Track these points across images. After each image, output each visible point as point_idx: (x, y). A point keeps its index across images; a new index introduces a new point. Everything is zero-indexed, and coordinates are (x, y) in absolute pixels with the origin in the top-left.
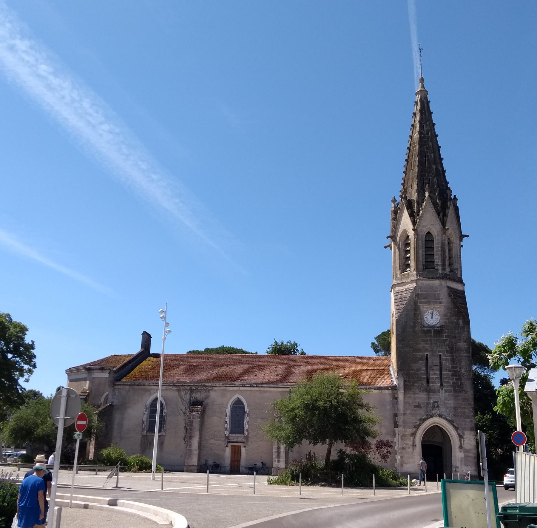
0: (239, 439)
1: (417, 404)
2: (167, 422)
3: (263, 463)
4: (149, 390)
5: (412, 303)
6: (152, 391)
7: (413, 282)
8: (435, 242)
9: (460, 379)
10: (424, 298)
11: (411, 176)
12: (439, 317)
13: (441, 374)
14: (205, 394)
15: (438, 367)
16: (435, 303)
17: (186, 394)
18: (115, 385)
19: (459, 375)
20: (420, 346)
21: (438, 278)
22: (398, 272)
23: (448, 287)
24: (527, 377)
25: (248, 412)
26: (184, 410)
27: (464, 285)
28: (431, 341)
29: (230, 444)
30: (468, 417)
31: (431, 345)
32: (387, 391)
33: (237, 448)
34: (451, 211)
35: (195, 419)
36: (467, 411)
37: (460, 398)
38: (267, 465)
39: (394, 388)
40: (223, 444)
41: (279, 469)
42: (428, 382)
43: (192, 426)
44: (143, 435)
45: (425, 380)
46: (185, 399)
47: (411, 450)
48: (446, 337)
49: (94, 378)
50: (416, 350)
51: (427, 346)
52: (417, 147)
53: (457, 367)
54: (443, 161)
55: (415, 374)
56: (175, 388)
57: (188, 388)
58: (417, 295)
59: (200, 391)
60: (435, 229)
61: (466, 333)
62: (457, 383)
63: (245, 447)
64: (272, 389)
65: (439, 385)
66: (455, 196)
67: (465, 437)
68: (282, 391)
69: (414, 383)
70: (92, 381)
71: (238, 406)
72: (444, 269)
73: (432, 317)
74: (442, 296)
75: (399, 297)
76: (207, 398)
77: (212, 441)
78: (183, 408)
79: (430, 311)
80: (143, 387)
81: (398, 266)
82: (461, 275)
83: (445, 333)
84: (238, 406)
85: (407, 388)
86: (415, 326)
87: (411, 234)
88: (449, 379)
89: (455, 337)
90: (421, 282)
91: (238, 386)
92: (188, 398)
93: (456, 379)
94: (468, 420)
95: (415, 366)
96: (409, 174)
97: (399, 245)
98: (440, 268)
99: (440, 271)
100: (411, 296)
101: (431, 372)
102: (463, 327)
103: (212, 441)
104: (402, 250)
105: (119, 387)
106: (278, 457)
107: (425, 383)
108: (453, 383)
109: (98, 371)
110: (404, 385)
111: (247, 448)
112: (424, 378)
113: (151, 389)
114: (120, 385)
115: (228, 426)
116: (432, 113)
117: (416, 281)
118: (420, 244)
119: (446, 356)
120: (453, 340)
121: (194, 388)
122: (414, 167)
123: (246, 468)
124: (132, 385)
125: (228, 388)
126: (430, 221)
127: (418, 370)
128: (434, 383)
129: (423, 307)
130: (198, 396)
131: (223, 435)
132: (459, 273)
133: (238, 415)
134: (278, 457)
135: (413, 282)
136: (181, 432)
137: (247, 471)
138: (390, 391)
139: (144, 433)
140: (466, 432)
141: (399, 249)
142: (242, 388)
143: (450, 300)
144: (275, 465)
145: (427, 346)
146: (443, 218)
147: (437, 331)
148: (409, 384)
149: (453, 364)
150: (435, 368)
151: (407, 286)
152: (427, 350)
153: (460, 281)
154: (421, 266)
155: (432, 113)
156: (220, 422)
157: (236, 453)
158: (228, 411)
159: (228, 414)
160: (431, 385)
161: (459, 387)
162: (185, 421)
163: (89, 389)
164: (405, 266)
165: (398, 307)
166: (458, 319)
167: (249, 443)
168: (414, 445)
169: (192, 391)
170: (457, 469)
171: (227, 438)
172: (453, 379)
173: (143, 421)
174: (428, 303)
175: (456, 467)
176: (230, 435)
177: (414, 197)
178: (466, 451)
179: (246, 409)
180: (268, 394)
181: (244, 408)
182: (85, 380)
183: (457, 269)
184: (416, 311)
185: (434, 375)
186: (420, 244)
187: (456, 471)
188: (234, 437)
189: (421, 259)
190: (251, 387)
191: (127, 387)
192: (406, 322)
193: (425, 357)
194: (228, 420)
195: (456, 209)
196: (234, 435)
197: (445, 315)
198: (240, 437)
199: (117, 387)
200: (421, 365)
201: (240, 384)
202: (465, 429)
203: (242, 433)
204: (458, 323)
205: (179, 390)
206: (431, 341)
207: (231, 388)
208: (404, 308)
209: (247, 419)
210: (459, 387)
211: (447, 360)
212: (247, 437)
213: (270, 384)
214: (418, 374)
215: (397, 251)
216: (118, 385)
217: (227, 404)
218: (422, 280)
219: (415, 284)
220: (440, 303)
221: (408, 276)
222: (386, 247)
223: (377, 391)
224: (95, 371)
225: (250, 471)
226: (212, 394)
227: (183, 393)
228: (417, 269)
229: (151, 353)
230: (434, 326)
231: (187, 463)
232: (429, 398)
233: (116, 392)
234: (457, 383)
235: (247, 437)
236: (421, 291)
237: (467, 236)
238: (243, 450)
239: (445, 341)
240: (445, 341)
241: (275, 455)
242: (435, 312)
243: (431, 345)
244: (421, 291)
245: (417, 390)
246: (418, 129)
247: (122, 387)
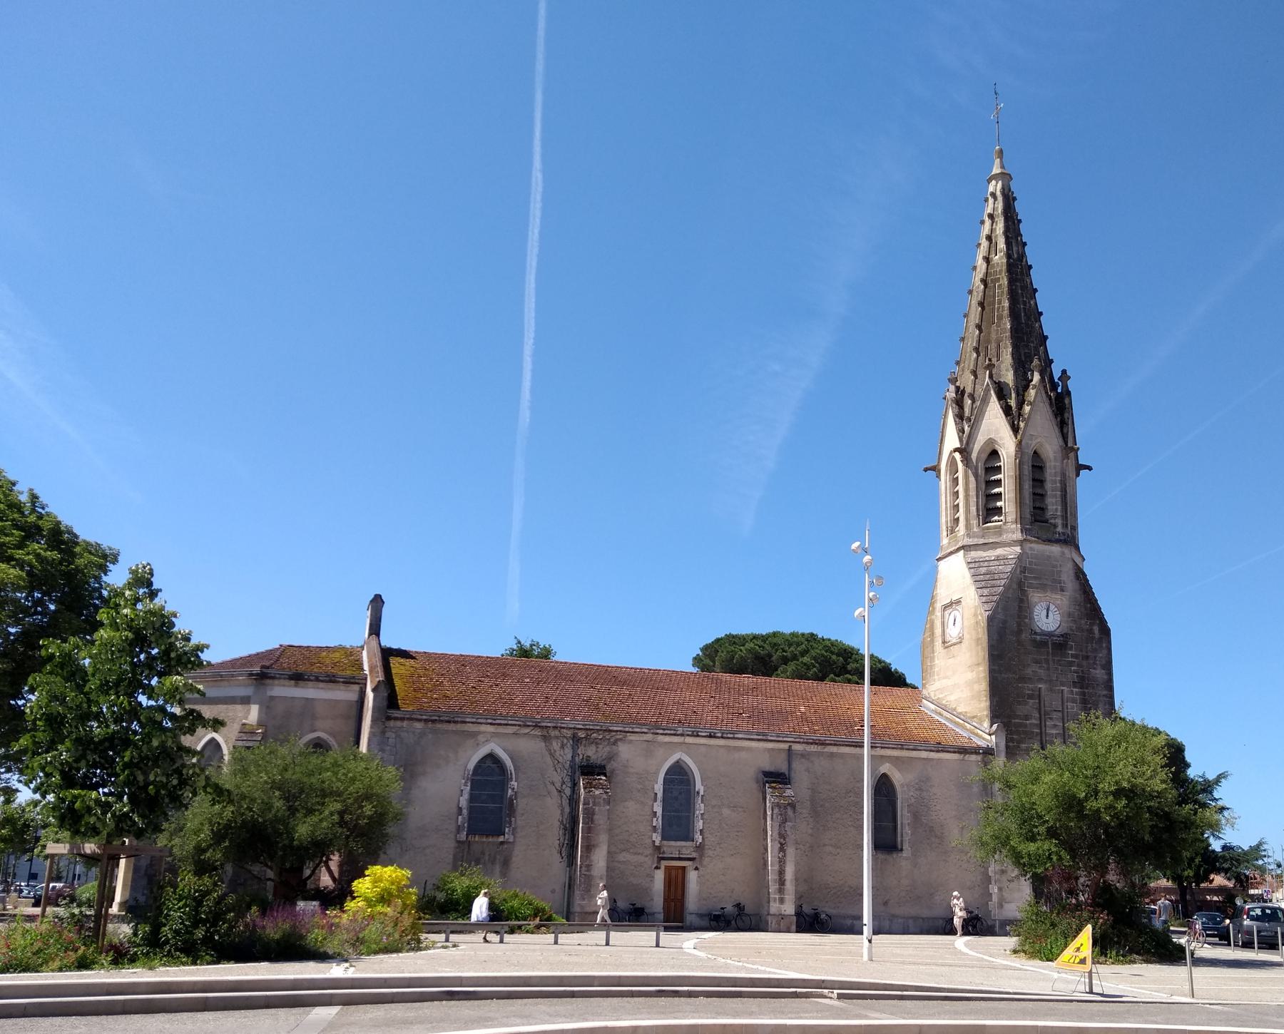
0: (684, 851)
2: (519, 810)
3: (738, 905)
4: (474, 735)
5: (1015, 586)
6: (481, 738)
7: (1015, 543)
10: (1035, 578)
11: (994, 336)
12: (1058, 618)
14: (607, 749)
16: (1053, 590)
17: (563, 747)
18: (389, 718)
20: (1029, 671)
21: (1057, 541)
22: (975, 522)
26: (558, 785)
28: (1047, 661)
29: (664, 863)
31: (1048, 669)
32: (973, 757)
33: (673, 873)
35: (599, 805)
38: (747, 910)
39: (988, 752)
40: (649, 862)
41: (783, 917)
43: (592, 821)
44: (459, 842)
46: (561, 759)
48: (1073, 656)
49: (272, 698)
50: (1023, 679)
51: (1042, 672)
52: (1005, 282)
55: (1020, 725)
56: (537, 732)
57: (569, 733)
58: (1024, 570)
59: (596, 742)
60: (1050, 447)
61: (1105, 652)
63: (696, 869)
64: (754, 744)
68: (769, 750)
69: (1019, 742)
70: (268, 706)
71: (678, 776)
73: (1048, 616)
74: (1064, 577)
75: (983, 570)
76: (611, 757)
78: (557, 779)
79: (1044, 604)
80: (459, 727)
81: (973, 509)
84: (678, 778)
85: (1011, 753)
86: (1020, 632)
90: (1029, 545)
91: (682, 735)
92: (569, 757)
95: (1021, 710)
96: (989, 333)
97: (976, 468)
98: (1059, 522)
99: (1060, 529)
100: (1014, 570)
102: (1100, 640)
104: (982, 479)
105: (399, 723)
106: (781, 890)
109: (287, 682)
110: (1007, 747)
113: (479, 733)
114: (402, 719)
115: (658, 822)
117: (1021, 543)
118: (1026, 472)
120: (1084, 663)
121: (581, 734)
122: (1000, 318)
123: (701, 916)
124: (434, 721)
125: (660, 738)
127: (1027, 717)
129: (1035, 596)
130: (592, 753)
131: (648, 841)
133: (676, 798)
134: (781, 890)
135: (1015, 543)
136: (554, 835)
137: (705, 923)
138: (979, 758)
139: (463, 836)
141: (976, 476)
142: (689, 740)
143: (1077, 586)
144: (774, 907)
147: (1057, 644)
150: (1055, 715)
151: (1000, 551)
152: (1040, 680)
154: (1028, 516)
156: (643, 811)
157: (675, 883)
158: (659, 788)
159: (660, 795)
162: (562, 811)
163: (260, 724)
164: (989, 510)
165: (986, 592)
166: (1092, 624)
167: (706, 861)
169: (576, 740)
171: (658, 848)
173: (460, 809)
174: (1043, 587)
176: (665, 842)
177: (1009, 377)
179: (699, 786)
180: (744, 755)
182: (246, 701)
184: (1021, 601)
186: (1026, 472)
188: (673, 847)
190: (710, 736)
191: (419, 725)
192: (1005, 622)
194: (658, 808)
196: (673, 843)
197: (1069, 615)
198: (686, 848)
199: (392, 723)
201: (688, 730)
203: (688, 837)
204: (1091, 631)
205: (546, 738)
206: (1047, 661)
207: (667, 739)
208: (1002, 594)
209: (700, 808)
211: (1074, 701)
212: (700, 848)
213: (751, 733)
214: (1026, 726)
215: (972, 479)
216: (396, 719)
217: (657, 773)
218: (1031, 542)
219: (1018, 549)
220: (1062, 590)
221: (999, 531)
222: (926, 470)
223: (956, 756)
224: (276, 682)
225: (713, 923)
226: (624, 751)
227: (556, 745)
228: (1021, 519)
230: (1050, 634)
231: (582, 907)
233: (388, 734)
235: (700, 848)
236: (1031, 563)
237: (1089, 468)
238: (692, 876)
239: (1071, 664)
240: (1071, 664)
241: (773, 888)
242: (1052, 607)
243: (1048, 669)
244: (1031, 563)
246: (1002, 244)
247: (405, 723)
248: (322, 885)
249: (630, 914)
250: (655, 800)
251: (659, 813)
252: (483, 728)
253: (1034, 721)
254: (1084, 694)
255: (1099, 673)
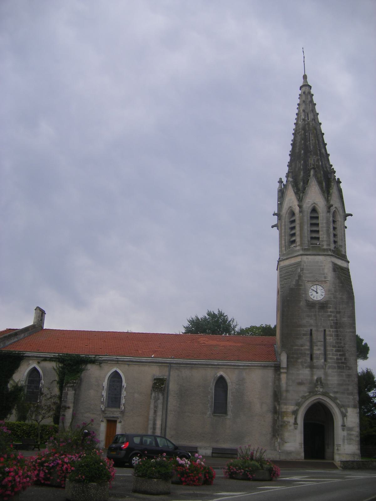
1: (300, 381)
8: (319, 218)
9: (343, 355)
13: (325, 350)
15: (322, 343)
19: (343, 351)
23: (333, 263)
24: (280, 366)
25: (125, 387)
27: (348, 262)
30: (352, 394)
34: (334, 191)
36: (350, 388)
37: (344, 374)
42: (312, 359)
45: (309, 356)
47: (292, 427)
48: (331, 312)
53: (341, 343)
54: (326, 147)
62: (341, 359)
65: (323, 361)
66: (338, 179)
67: (348, 414)
72: (329, 245)
74: (326, 271)
77: (354, 349)
82: (345, 252)
83: (330, 308)
87: (297, 210)
88: (333, 355)
89: (339, 312)
93: (340, 355)
94: (351, 397)
101: (315, 348)
103: (354, 349)
107: (308, 359)
108: (337, 359)
111: (123, 423)
112: (308, 354)
116: (315, 104)
119: (330, 331)
120: (338, 315)
126: (314, 195)
127: (302, 346)
128: (318, 358)
132: (343, 250)
133: (115, 389)
140: (350, 410)
145: (312, 322)
146: (328, 197)
147: (323, 306)
148: (292, 360)
149: (338, 339)
150: (319, 343)
153: (343, 257)
155: (315, 104)
158: (105, 384)
160: (315, 361)
161: (342, 363)
168: (296, 423)
170: (339, 448)
172: (337, 355)
175: (339, 445)
176: (107, 409)
178: (350, 429)
179: (124, 384)
181: (121, 381)
183: (341, 246)
185: (318, 351)
187: (338, 449)
189: (306, 235)
193: (309, 332)
194: (104, 393)
195: (340, 191)
200: (305, 341)
202: (349, 406)
203: (119, 407)
206: (315, 315)
209: (124, 393)
210: (342, 363)
211: (331, 335)
212: (123, 412)
217: (104, 378)
222: (273, 227)
229: (44, 328)
232: (312, 375)
234: (341, 359)
235: (123, 412)
237: (351, 215)
239: (330, 316)
240: (330, 316)
245: (301, 366)
248: (35, 480)
249: (164, 395)
250: (103, 389)
251: (105, 396)
252: (32, 385)
253: (307, 347)
254: (337, 331)
255: (345, 320)
